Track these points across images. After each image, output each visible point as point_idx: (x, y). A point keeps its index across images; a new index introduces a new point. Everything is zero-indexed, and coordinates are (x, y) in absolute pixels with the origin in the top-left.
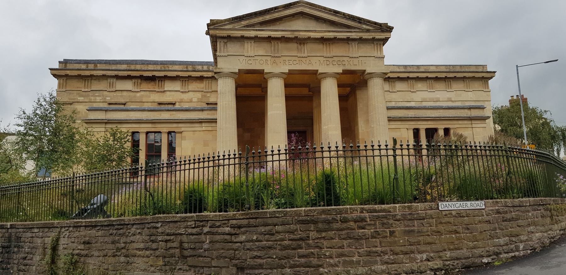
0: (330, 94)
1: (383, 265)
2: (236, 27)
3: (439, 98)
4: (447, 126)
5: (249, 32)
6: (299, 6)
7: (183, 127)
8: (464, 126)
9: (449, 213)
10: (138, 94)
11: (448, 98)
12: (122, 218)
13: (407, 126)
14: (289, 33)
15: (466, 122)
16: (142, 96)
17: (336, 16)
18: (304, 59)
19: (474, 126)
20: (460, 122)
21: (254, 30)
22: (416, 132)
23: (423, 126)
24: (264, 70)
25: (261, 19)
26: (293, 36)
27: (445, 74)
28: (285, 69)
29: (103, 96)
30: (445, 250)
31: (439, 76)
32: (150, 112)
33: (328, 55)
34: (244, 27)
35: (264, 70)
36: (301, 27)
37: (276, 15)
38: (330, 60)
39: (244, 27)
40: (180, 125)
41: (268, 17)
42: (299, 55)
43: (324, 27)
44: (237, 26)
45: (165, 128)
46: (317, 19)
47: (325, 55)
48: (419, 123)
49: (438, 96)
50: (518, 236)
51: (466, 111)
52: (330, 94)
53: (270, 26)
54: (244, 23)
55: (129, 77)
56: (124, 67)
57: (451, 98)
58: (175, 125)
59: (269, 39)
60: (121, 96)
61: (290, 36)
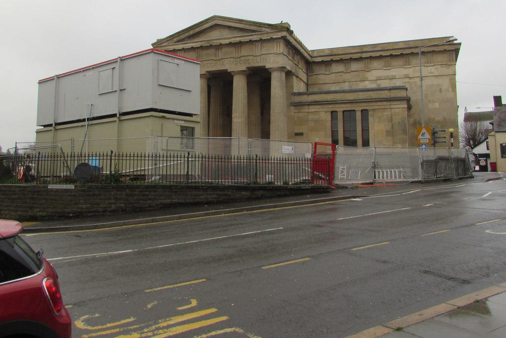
0: (240, 86)
4: (365, 108)
5: (178, 46)
6: (214, 20)
7: (375, 106)
8: (383, 107)
9: (52, 190)
11: (405, 75)
13: (326, 110)
15: (385, 103)
18: (218, 62)
19: (392, 107)
20: (379, 104)
21: (181, 44)
22: (333, 114)
23: (340, 109)
24: (227, 70)
25: (187, 34)
30: (48, 208)
31: (394, 54)
33: (237, 56)
35: (227, 70)
36: (216, 37)
37: (197, 30)
38: (239, 60)
41: (191, 33)
42: (215, 58)
43: (236, 34)
45: (358, 108)
46: (229, 27)
47: (234, 55)
48: (337, 106)
49: (394, 74)
50: (98, 204)
51: (386, 91)
52: (240, 86)
54: (175, 39)
59: (192, 49)
61: (207, 45)
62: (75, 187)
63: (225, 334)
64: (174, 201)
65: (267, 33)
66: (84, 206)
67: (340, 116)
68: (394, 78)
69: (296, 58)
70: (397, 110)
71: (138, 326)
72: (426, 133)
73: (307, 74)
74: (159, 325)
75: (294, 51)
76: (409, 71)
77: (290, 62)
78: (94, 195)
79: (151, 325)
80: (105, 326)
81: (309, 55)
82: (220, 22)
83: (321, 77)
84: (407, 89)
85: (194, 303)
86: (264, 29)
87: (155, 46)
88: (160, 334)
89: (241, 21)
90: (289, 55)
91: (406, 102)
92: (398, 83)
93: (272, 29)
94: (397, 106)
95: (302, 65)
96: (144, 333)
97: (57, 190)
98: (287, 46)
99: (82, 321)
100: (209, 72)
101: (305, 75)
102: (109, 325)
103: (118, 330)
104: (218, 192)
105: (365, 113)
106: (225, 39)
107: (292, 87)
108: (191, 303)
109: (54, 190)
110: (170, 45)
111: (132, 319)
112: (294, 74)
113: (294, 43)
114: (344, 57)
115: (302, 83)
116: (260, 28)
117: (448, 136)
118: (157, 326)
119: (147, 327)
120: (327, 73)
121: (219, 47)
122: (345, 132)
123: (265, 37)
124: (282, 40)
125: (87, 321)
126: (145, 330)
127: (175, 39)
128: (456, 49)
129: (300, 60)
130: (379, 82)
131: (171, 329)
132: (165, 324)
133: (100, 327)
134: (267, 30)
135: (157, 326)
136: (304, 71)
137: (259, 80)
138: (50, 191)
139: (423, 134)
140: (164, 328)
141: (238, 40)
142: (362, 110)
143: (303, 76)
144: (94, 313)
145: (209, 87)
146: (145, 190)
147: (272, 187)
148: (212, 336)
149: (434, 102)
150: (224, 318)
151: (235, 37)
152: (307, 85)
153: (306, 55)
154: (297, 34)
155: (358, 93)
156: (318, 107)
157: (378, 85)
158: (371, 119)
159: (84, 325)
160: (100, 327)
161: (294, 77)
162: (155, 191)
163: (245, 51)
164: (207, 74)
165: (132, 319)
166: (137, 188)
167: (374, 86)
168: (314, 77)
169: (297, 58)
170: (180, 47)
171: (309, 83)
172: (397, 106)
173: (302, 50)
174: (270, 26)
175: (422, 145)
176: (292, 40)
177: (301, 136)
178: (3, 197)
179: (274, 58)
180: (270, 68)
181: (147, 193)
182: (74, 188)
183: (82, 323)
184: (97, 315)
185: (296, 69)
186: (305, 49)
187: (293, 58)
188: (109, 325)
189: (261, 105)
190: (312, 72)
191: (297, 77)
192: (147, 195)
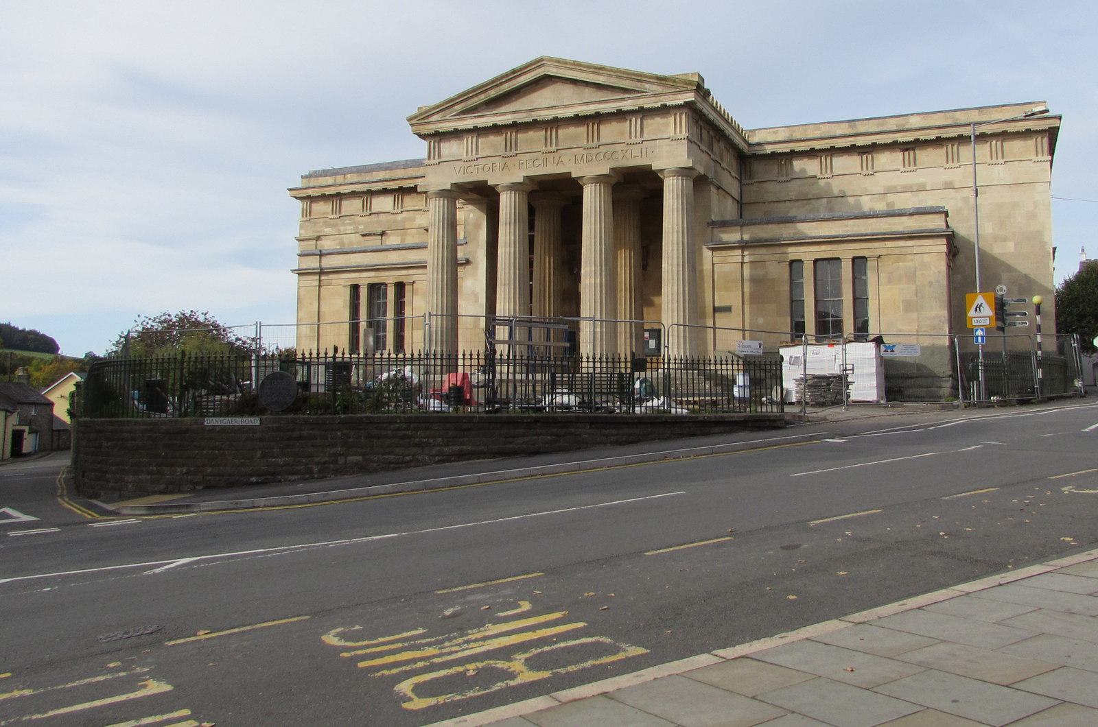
0: (593, 202)
1: (148, 475)
2: (447, 117)
3: (924, 185)
5: (465, 122)
8: (897, 251)
9: (213, 429)
10: (400, 217)
11: (946, 183)
12: (499, 415)
14: (524, 115)
16: (404, 220)
17: (599, 74)
19: (916, 250)
20: (889, 244)
23: (364, 279)
24: (570, 173)
25: (482, 98)
26: (530, 120)
27: (936, 131)
28: (519, 178)
29: (355, 223)
31: (922, 138)
32: (374, 253)
34: (458, 114)
35: (570, 173)
36: (545, 103)
37: (506, 87)
38: (594, 151)
39: (458, 114)
40: (411, 272)
41: (493, 93)
43: (590, 94)
44: (449, 114)
48: (802, 249)
49: (922, 180)
53: (501, 105)
54: (458, 108)
55: (385, 192)
56: (381, 175)
57: (951, 183)
58: (404, 272)
59: (496, 129)
60: (378, 222)
62: (261, 420)
63: (582, 645)
64: (464, 447)
65: (655, 95)
66: (280, 461)
67: (364, 293)
68: (922, 189)
69: (716, 147)
70: (926, 258)
71: (433, 640)
72: (985, 305)
73: (740, 181)
74: (469, 637)
75: (711, 133)
76: (959, 175)
77: (704, 157)
78: (300, 438)
79: (455, 638)
80: (375, 642)
81: (744, 140)
82: (553, 71)
83: (771, 187)
84: (947, 214)
85: (526, 606)
86: (647, 86)
87: (414, 122)
88: (472, 648)
89: (599, 69)
90: (701, 140)
91: (944, 241)
92: (929, 201)
93: (665, 85)
94: (927, 250)
95: (729, 161)
96: (445, 647)
97: (224, 430)
98: (697, 122)
99: (335, 636)
100: (530, 179)
101: (736, 184)
102: (381, 640)
103: (400, 645)
104: (555, 430)
105: (859, 263)
106: (565, 106)
107: (708, 209)
108: (519, 606)
109: (218, 429)
110: (449, 121)
111: (421, 631)
112: (712, 183)
113: (712, 116)
114: (818, 145)
115: (730, 201)
116: (639, 84)
117: (1030, 312)
118: (465, 638)
119: (449, 639)
120: (784, 179)
121: (555, 123)
122: (819, 304)
123: (648, 103)
124: (686, 110)
125: (342, 636)
126: (446, 644)
127: (458, 108)
128: (1050, 128)
129: (725, 153)
130: (891, 198)
131: (489, 642)
132: (479, 635)
133: (367, 642)
134: (654, 87)
135: (465, 638)
136: (733, 174)
137: (637, 193)
138: (210, 430)
139: (978, 308)
140: (476, 640)
141: (591, 109)
142: (854, 259)
143: (733, 187)
144: (352, 624)
145: (532, 212)
146: (405, 426)
147: (666, 418)
148: (560, 648)
149: (1005, 240)
150: (581, 625)
151: (587, 103)
152: (741, 204)
153: (737, 140)
154: (717, 96)
155: (845, 222)
156: (763, 251)
157: (888, 204)
158: (871, 277)
159: (339, 640)
160: (367, 642)
161: (713, 189)
162: (427, 429)
163: (608, 131)
164: (527, 182)
165: (421, 631)
166: (390, 423)
167: (880, 207)
168: (755, 188)
169: (719, 147)
170: (469, 123)
171: (744, 202)
172: (927, 250)
173: (729, 131)
174: (662, 80)
175: (976, 330)
176: (707, 110)
177: (727, 314)
178: (109, 444)
179: (667, 149)
180: (662, 170)
181: (409, 433)
182: (258, 424)
183: (336, 639)
184: (357, 627)
185: (716, 172)
186: (737, 130)
187: (710, 146)
188: (381, 640)
189: (643, 248)
190: (751, 177)
191: (719, 188)
192: (409, 437)
